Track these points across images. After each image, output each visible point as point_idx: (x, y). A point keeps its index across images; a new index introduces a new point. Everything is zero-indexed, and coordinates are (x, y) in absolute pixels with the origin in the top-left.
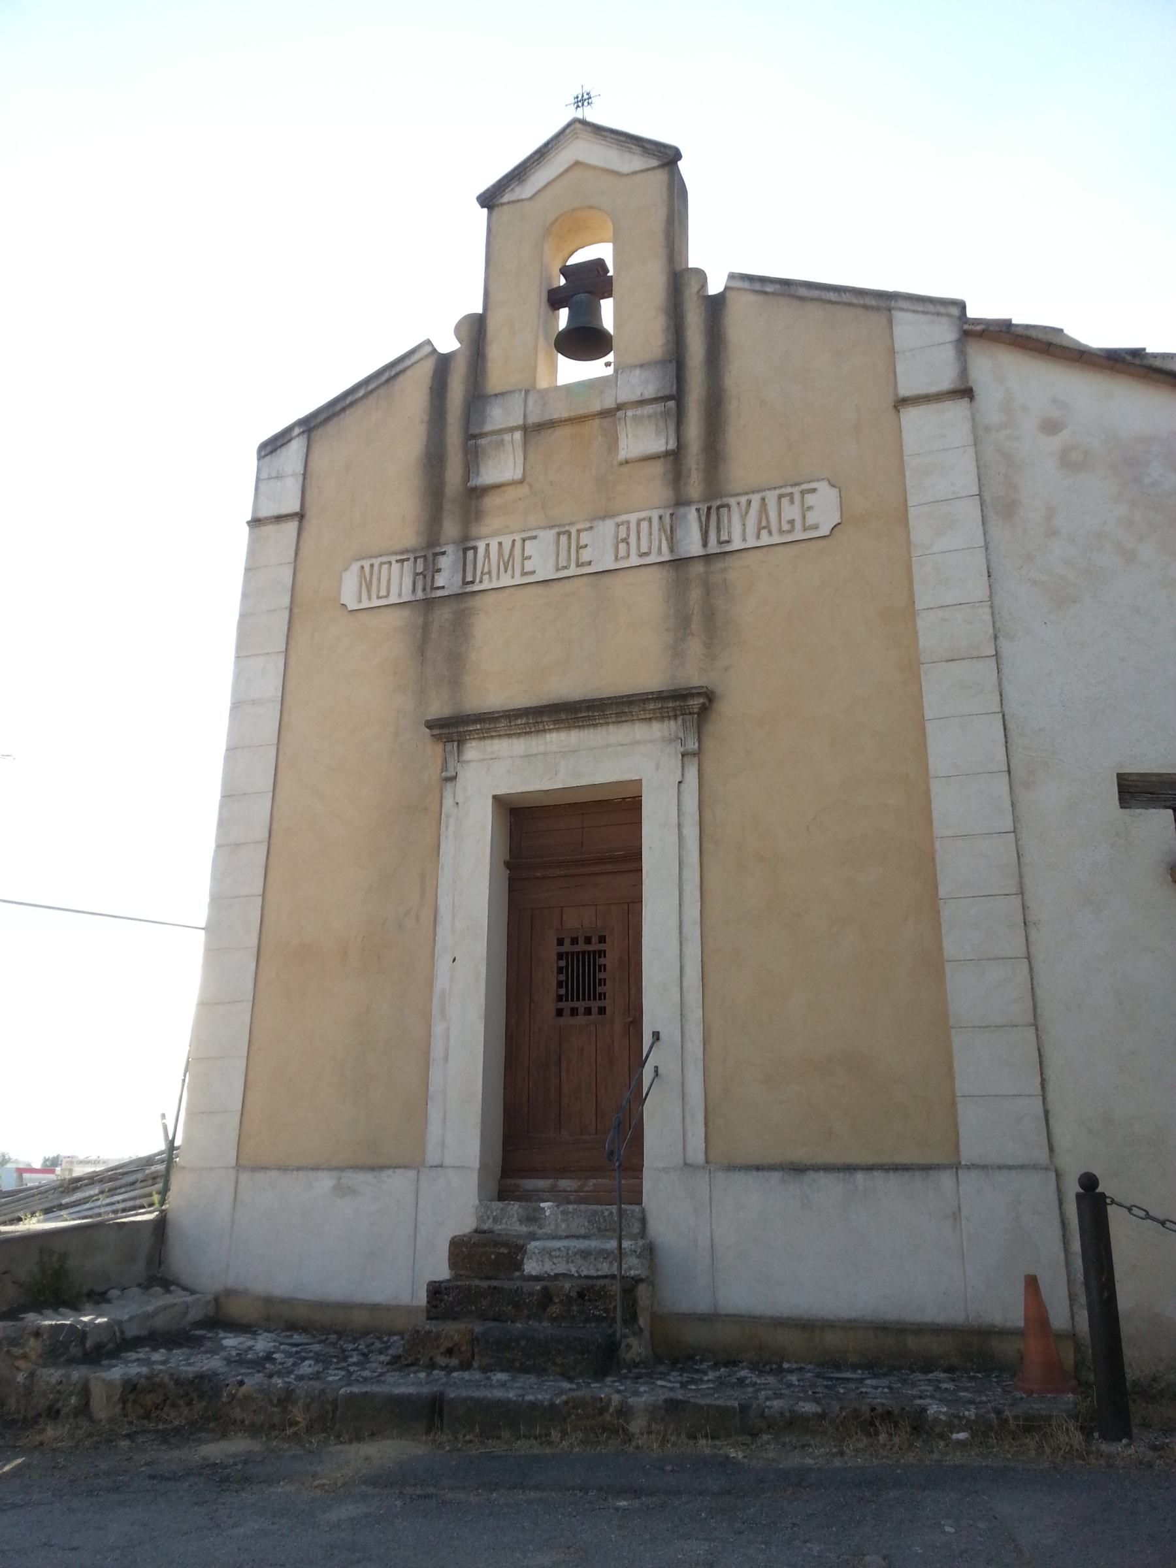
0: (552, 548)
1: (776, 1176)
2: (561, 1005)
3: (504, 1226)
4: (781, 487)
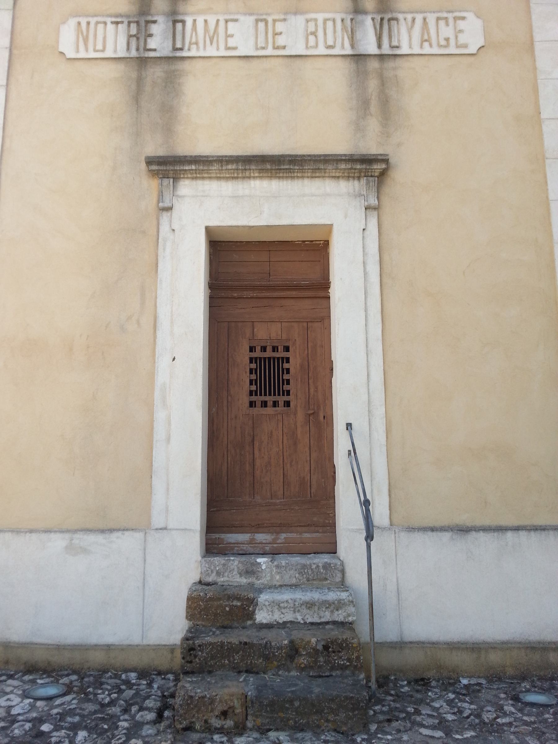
0: (252, 31)
1: (446, 536)
2: (254, 398)
3: (226, 579)
4: (439, 12)
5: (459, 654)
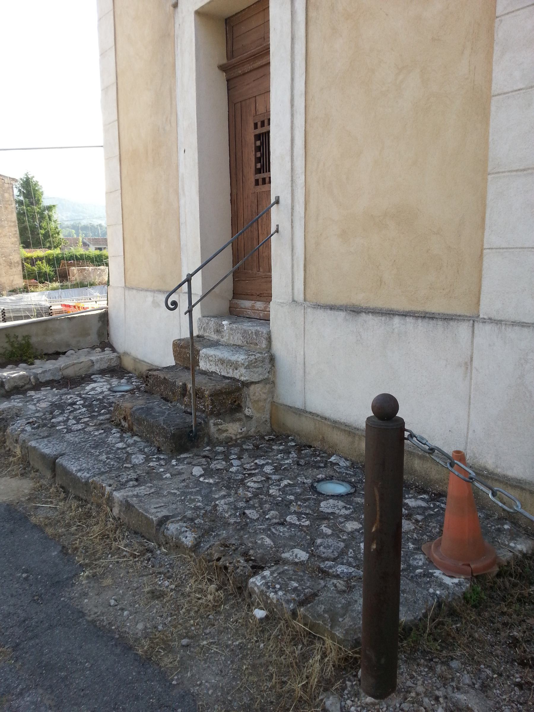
5: (339, 434)
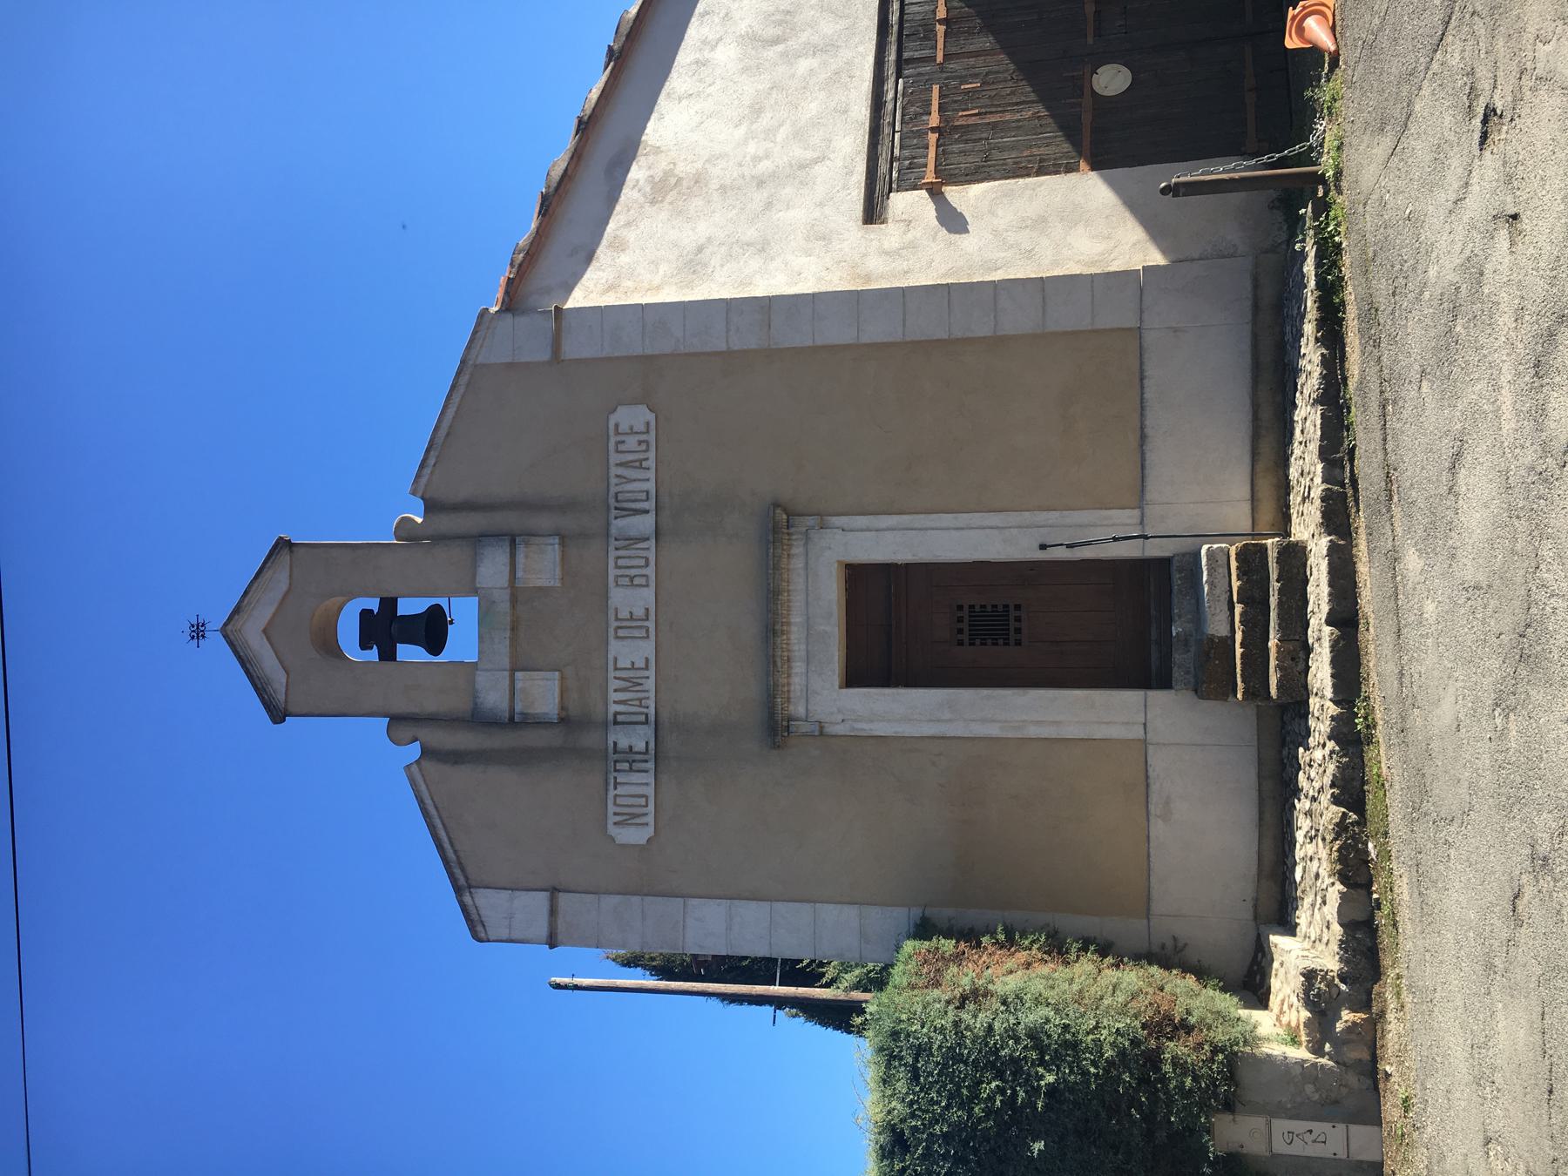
0: (625, 642)
2: (1012, 641)
